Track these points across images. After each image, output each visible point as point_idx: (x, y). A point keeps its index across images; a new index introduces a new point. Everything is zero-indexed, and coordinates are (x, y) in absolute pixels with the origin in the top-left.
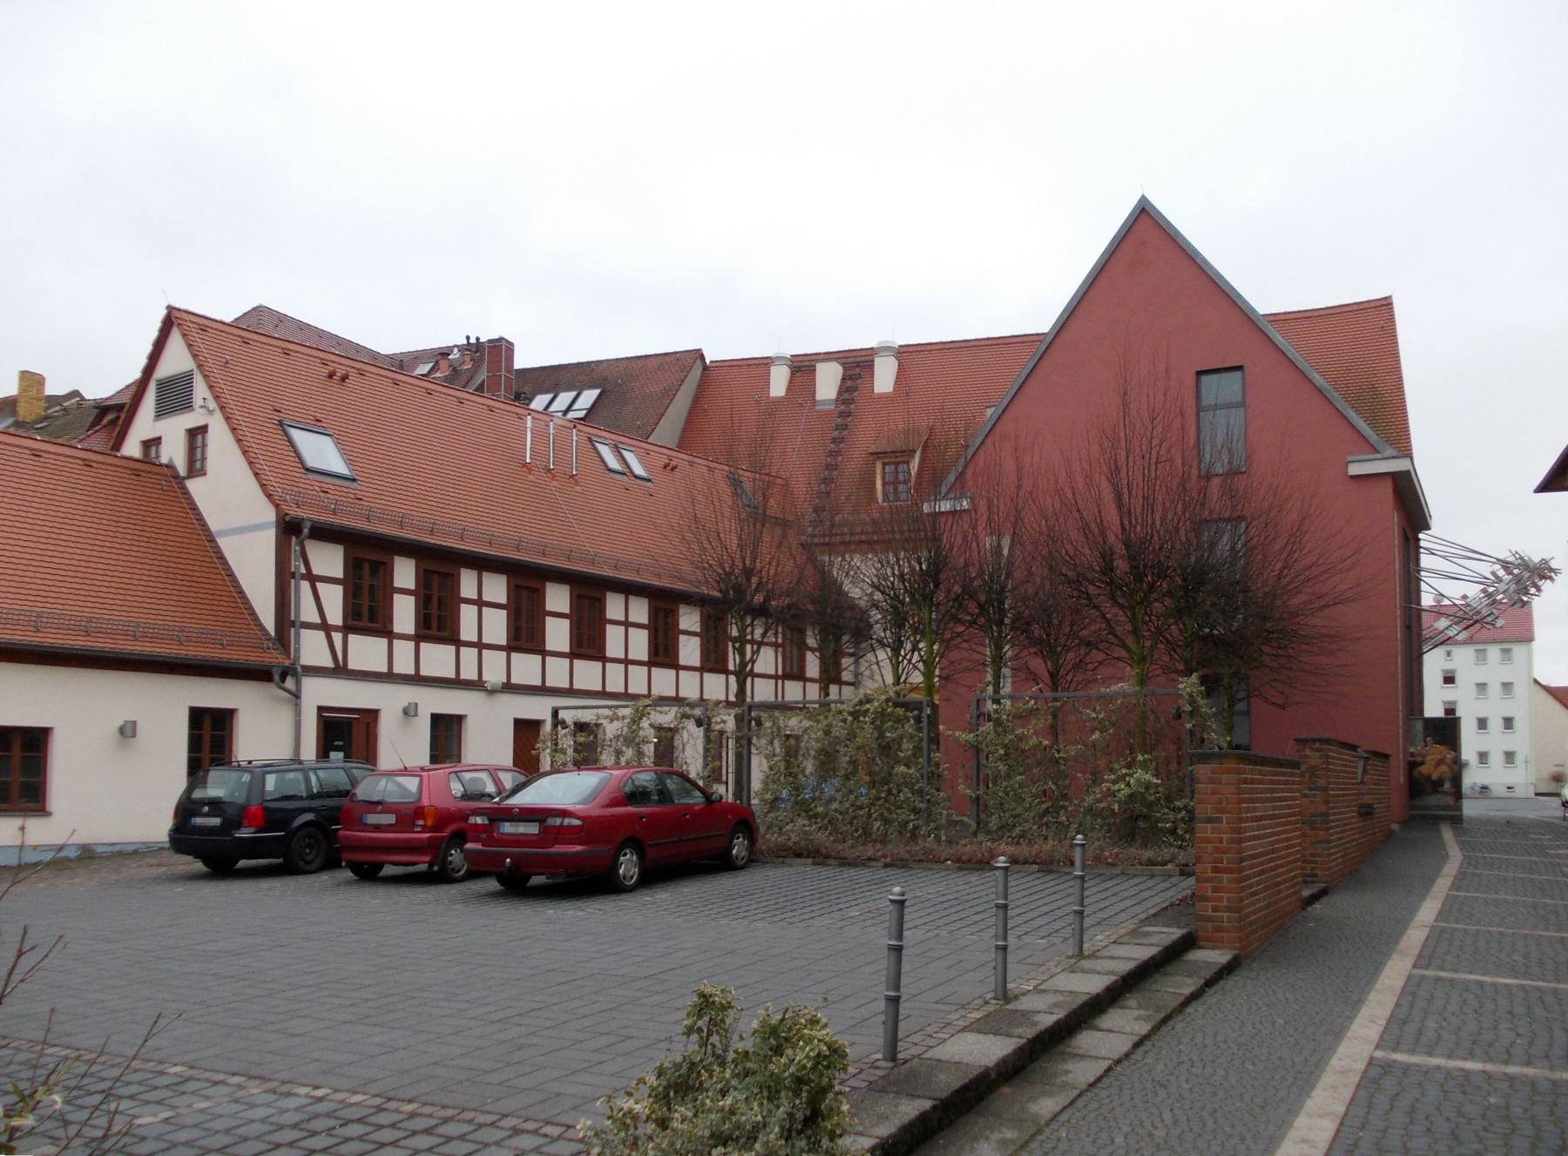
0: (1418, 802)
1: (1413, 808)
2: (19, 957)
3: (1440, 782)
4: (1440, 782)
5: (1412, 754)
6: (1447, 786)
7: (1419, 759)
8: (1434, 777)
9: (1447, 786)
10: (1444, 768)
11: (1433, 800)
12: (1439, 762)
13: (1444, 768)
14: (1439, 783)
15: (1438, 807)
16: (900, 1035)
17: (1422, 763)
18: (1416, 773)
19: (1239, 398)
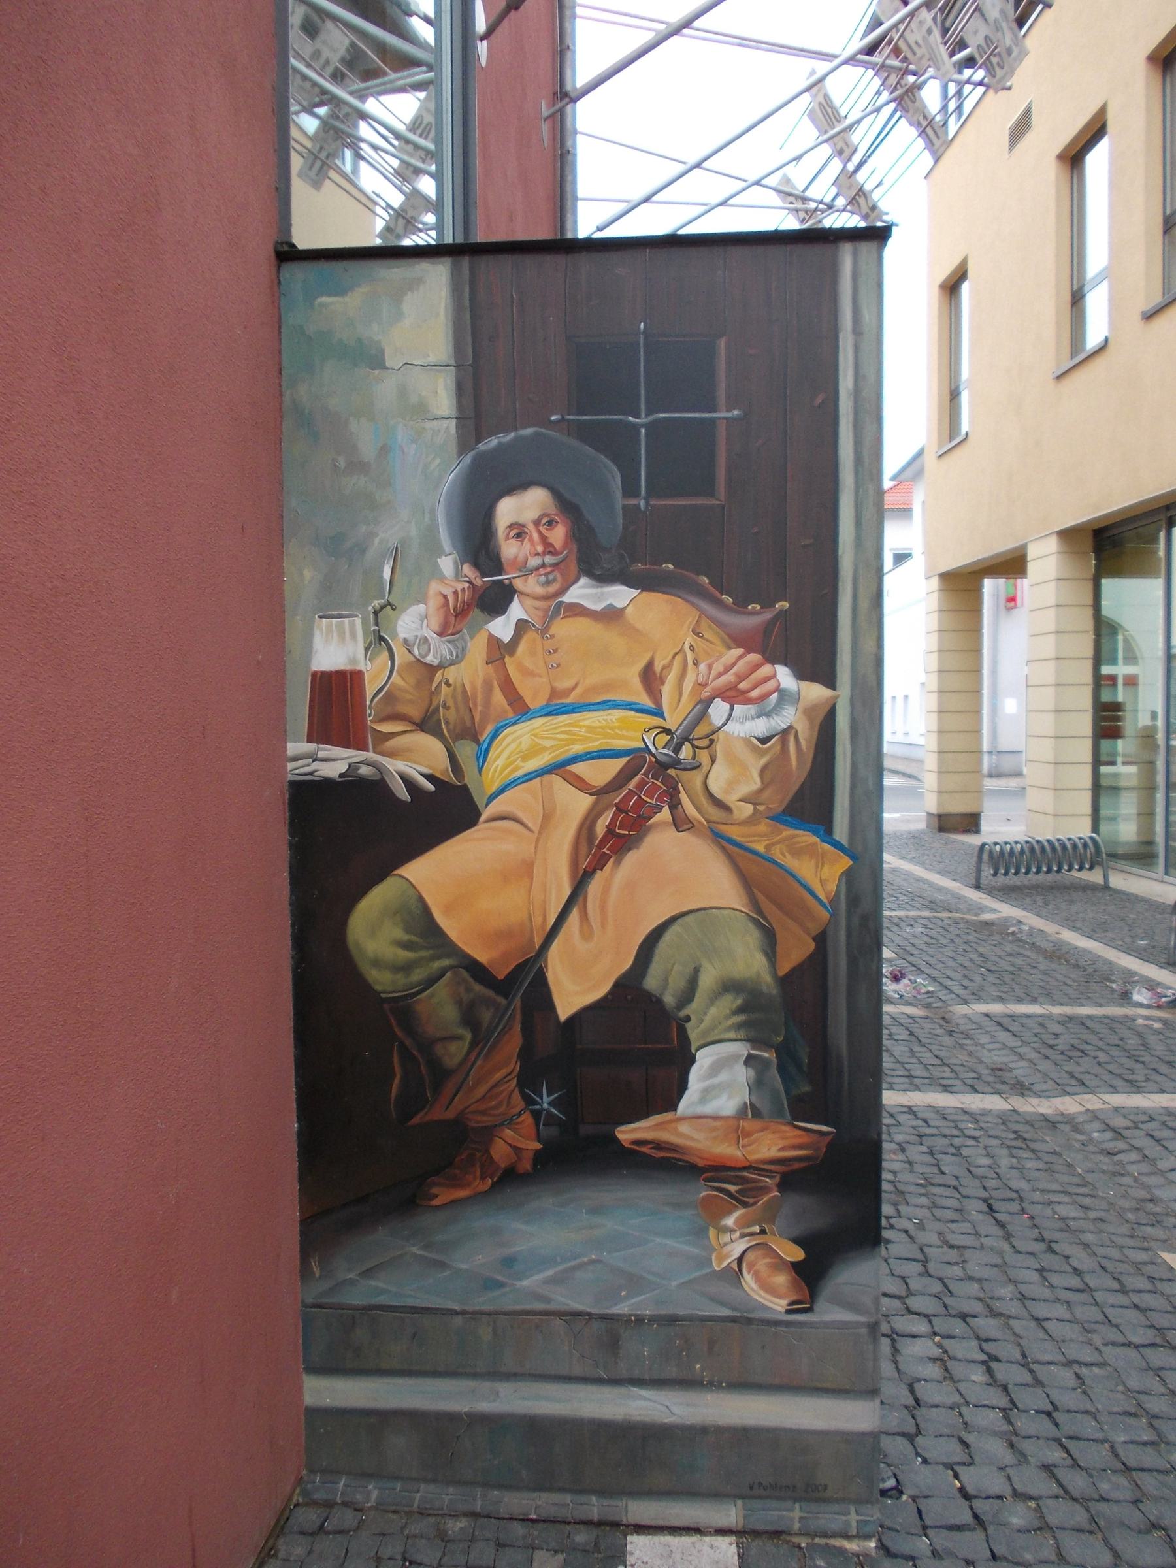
0: (393, 1274)
1: (342, 1343)
2: (723, 203)
3: (637, 1044)
4: (637, 1044)
5: (337, 704)
6: (719, 1085)
7: (411, 761)
8: (576, 984)
9: (719, 1085)
10: (679, 876)
11: (559, 1249)
12: (640, 796)
13: (679, 876)
14: (627, 1051)
15: (606, 1343)
16: (696, 24)
17: (447, 810)
18: (373, 930)
19: (303, 240)
